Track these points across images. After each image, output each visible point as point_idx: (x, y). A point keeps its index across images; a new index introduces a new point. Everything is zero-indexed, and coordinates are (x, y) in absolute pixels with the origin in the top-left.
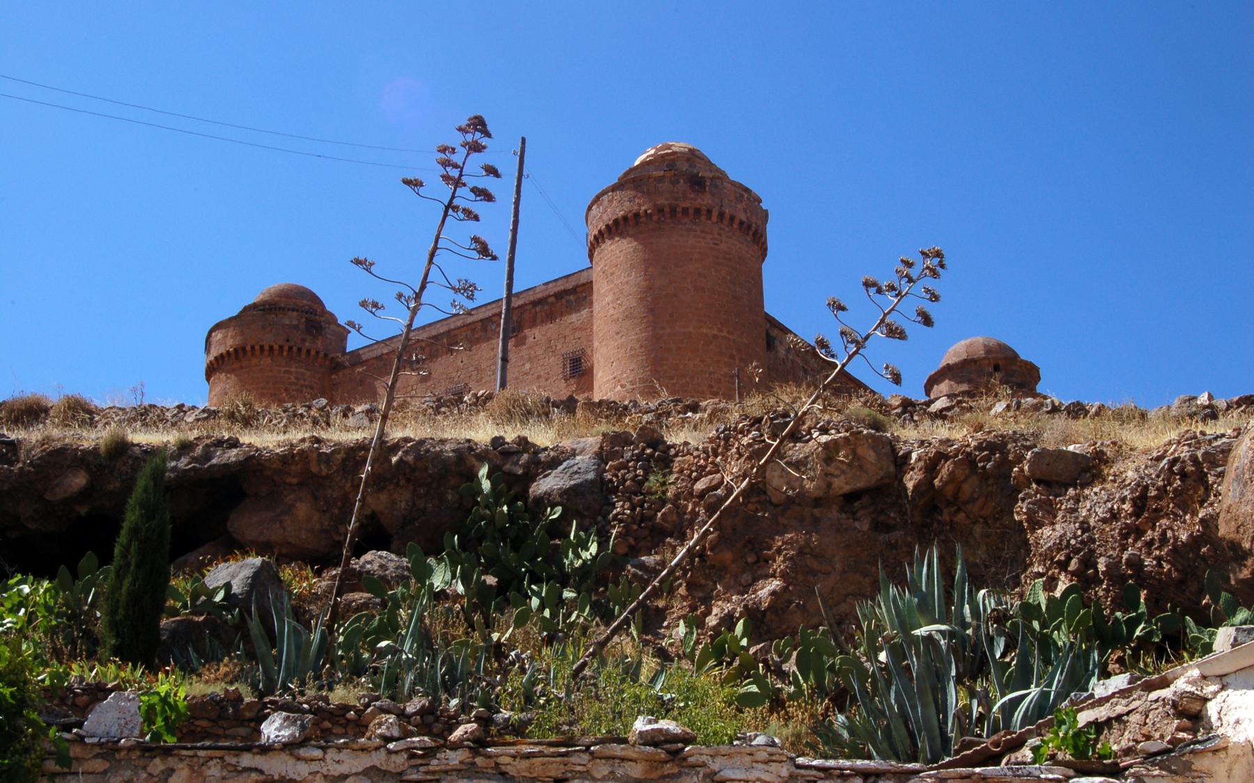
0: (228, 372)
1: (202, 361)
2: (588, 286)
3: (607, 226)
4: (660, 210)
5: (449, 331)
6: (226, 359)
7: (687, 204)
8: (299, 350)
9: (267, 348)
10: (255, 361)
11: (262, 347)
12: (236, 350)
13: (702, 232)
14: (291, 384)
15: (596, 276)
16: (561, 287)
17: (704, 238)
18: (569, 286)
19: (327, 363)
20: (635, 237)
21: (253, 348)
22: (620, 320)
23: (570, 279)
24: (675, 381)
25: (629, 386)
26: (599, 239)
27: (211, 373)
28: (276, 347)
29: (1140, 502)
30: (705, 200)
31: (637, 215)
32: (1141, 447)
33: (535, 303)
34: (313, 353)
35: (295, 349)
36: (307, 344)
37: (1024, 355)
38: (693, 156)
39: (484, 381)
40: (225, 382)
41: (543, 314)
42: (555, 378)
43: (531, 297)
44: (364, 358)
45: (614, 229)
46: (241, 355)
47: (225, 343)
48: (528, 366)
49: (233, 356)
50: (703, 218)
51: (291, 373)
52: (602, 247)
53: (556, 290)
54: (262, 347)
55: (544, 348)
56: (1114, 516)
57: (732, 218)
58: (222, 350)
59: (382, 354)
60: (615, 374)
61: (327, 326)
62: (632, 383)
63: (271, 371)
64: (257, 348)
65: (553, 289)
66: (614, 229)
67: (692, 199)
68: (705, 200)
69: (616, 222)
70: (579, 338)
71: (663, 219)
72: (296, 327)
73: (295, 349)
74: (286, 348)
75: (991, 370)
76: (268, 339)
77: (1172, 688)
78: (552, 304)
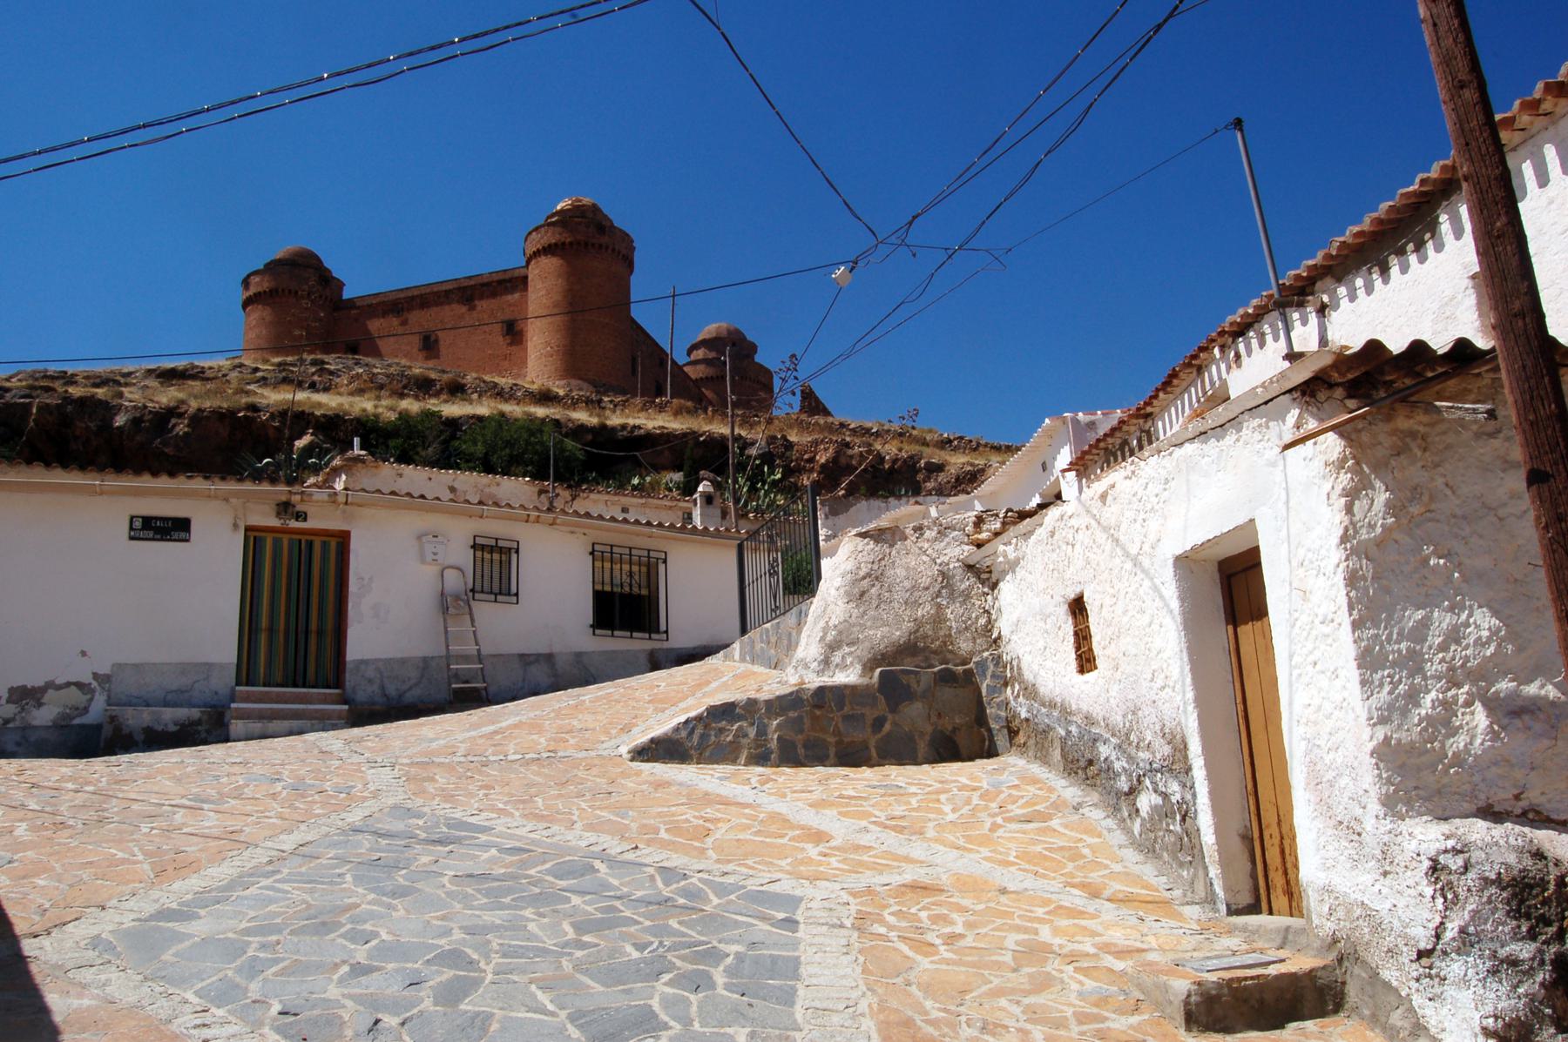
0: (264, 305)
1: (241, 296)
3: (543, 247)
4: (579, 243)
12: (270, 291)
16: (501, 277)
18: (507, 276)
21: (283, 290)
25: (556, 348)
26: (537, 254)
29: (957, 479)
30: (605, 240)
31: (564, 244)
33: (483, 285)
37: (750, 337)
38: (595, 208)
43: (480, 281)
44: (358, 304)
45: (547, 250)
56: (949, 482)
57: (619, 252)
65: (495, 278)
66: (547, 250)
68: (605, 240)
69: (550, 246)
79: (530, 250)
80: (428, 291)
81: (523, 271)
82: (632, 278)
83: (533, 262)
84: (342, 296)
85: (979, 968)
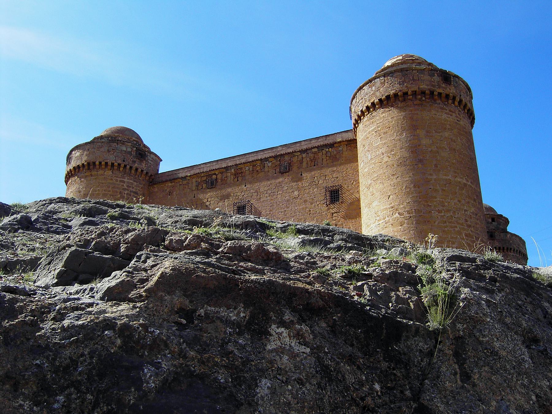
1: (64, 169)
2: (353, 143)
3: (380, 100)
5: (236, 165)
6: (81, 168)
7: (441, 91)
8: (131, 168)
9: (110, 164)
10: (101, 172)
11: (106, 163)
12: (89, 164)
13: (450, 111)
14: (125, 189)
15: (360, 138)
16: (321, 143)
17: (451, 115)
18: (329, 141)
19: (147, 178)
20: (401, 109)
21: (100, 163)
22: (395, 166)
23: (328, 138)
24: (443, 214)
27: (70, 177)
28: (116, 164)
31: (405, 94)
32: (530, 264)
34: (140, 170)
35: (128, 167)
36: (136, 165)
39: (262, 200)
40: (77, 184)
41: (308, 159)
42: (318, 203)
46: (91, 167)
47: (82, 158)
48: (296, 193)
49: (86, 167)
50: (450, 101)
51: (124, 182)
52: (373, 114)
53: (319, 144)
54: (106, 163)
55: (309, 181)
58: (79, 163)
59: (187, 176)
60: (393, 204)
61: (149, 154)
62: (408, 212)
63: (112, 179)
64: (103, 163)
67: (443, 88)
68: (451, 90)
69: (388, 97)
70: (337, 178)
71: (424, 98)
72: (130, 153)
73: (128, 167)
74: (123, 165)
75: (490, 220)
76: (111, 158)
77: (74, 209)
78: (315, 153)
79: (360, 105)
80: (243, 161)
81: (350, 136)
82: (473, 131)
83: (365, 119)
84: (158, 170)
85: (16, 294)
